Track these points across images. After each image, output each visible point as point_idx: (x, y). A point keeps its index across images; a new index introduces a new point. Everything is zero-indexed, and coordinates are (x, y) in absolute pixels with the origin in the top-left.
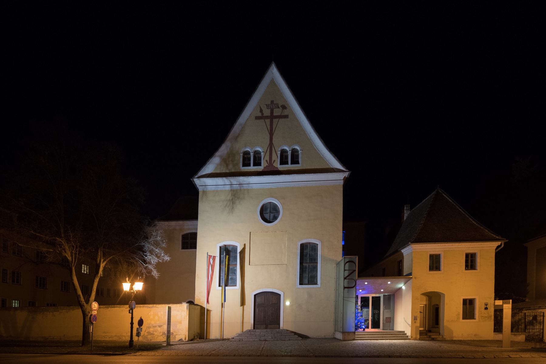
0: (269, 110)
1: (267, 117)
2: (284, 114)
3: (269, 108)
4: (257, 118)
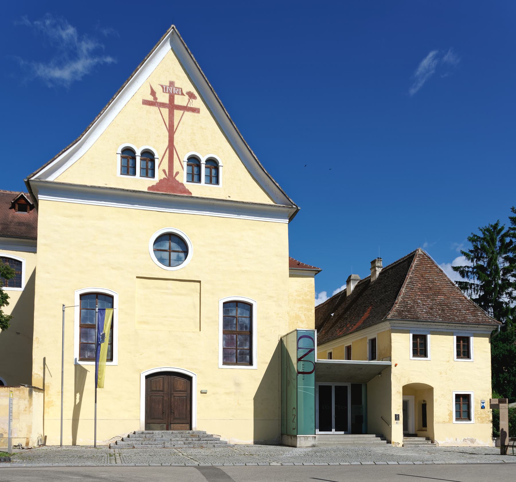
0: (167, 95)
1: (163, 105)
2: (192, 106)
3: (167, 91)
4: (146, 102)
